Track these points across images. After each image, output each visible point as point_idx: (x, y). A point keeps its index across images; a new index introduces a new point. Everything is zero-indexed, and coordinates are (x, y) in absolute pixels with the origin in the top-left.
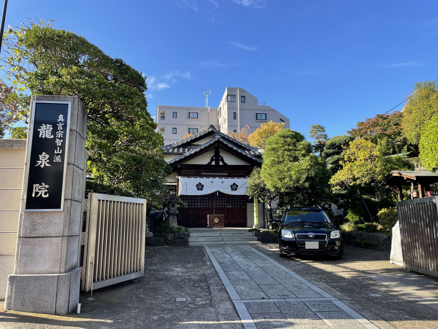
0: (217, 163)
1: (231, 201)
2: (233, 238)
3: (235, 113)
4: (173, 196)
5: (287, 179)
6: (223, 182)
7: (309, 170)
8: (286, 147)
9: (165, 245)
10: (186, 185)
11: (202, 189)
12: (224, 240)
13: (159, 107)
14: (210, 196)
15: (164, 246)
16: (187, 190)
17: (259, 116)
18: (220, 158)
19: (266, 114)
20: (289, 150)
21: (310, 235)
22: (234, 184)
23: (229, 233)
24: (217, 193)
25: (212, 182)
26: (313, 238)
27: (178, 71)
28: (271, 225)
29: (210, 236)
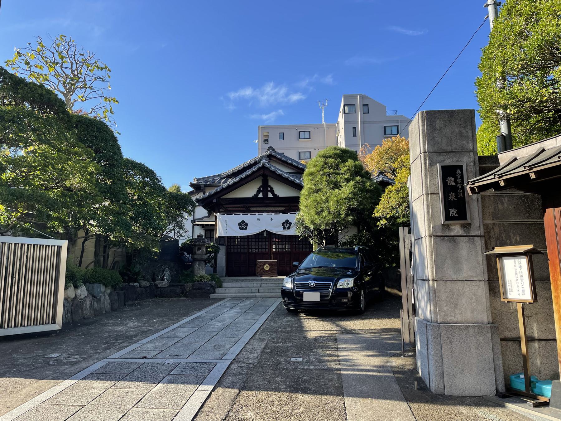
0: (265, 195)
2: (271, 289)
3: (355, 129)
4: (200, 238)
5: (325, 213)
6: (272, 219)
7: (350, 199)
8: (326, 170)
9: (182, 297)
10: (226, 224)
11: (245, 229)
12: (260, 292)
13: (261, 127)
14: (253, 237)
15: (181, 297)
16: (226, 229)
17: (388, 130)
18: (269, 189)
19: (398, 126)
20: (329, 175)
21: (310, 284)
22: (287, 221)
23: (272, 284)
24: (265, 233)
25: (258, 219)
26: (314, 287)
27: (316, 76)
29: (248, 286)
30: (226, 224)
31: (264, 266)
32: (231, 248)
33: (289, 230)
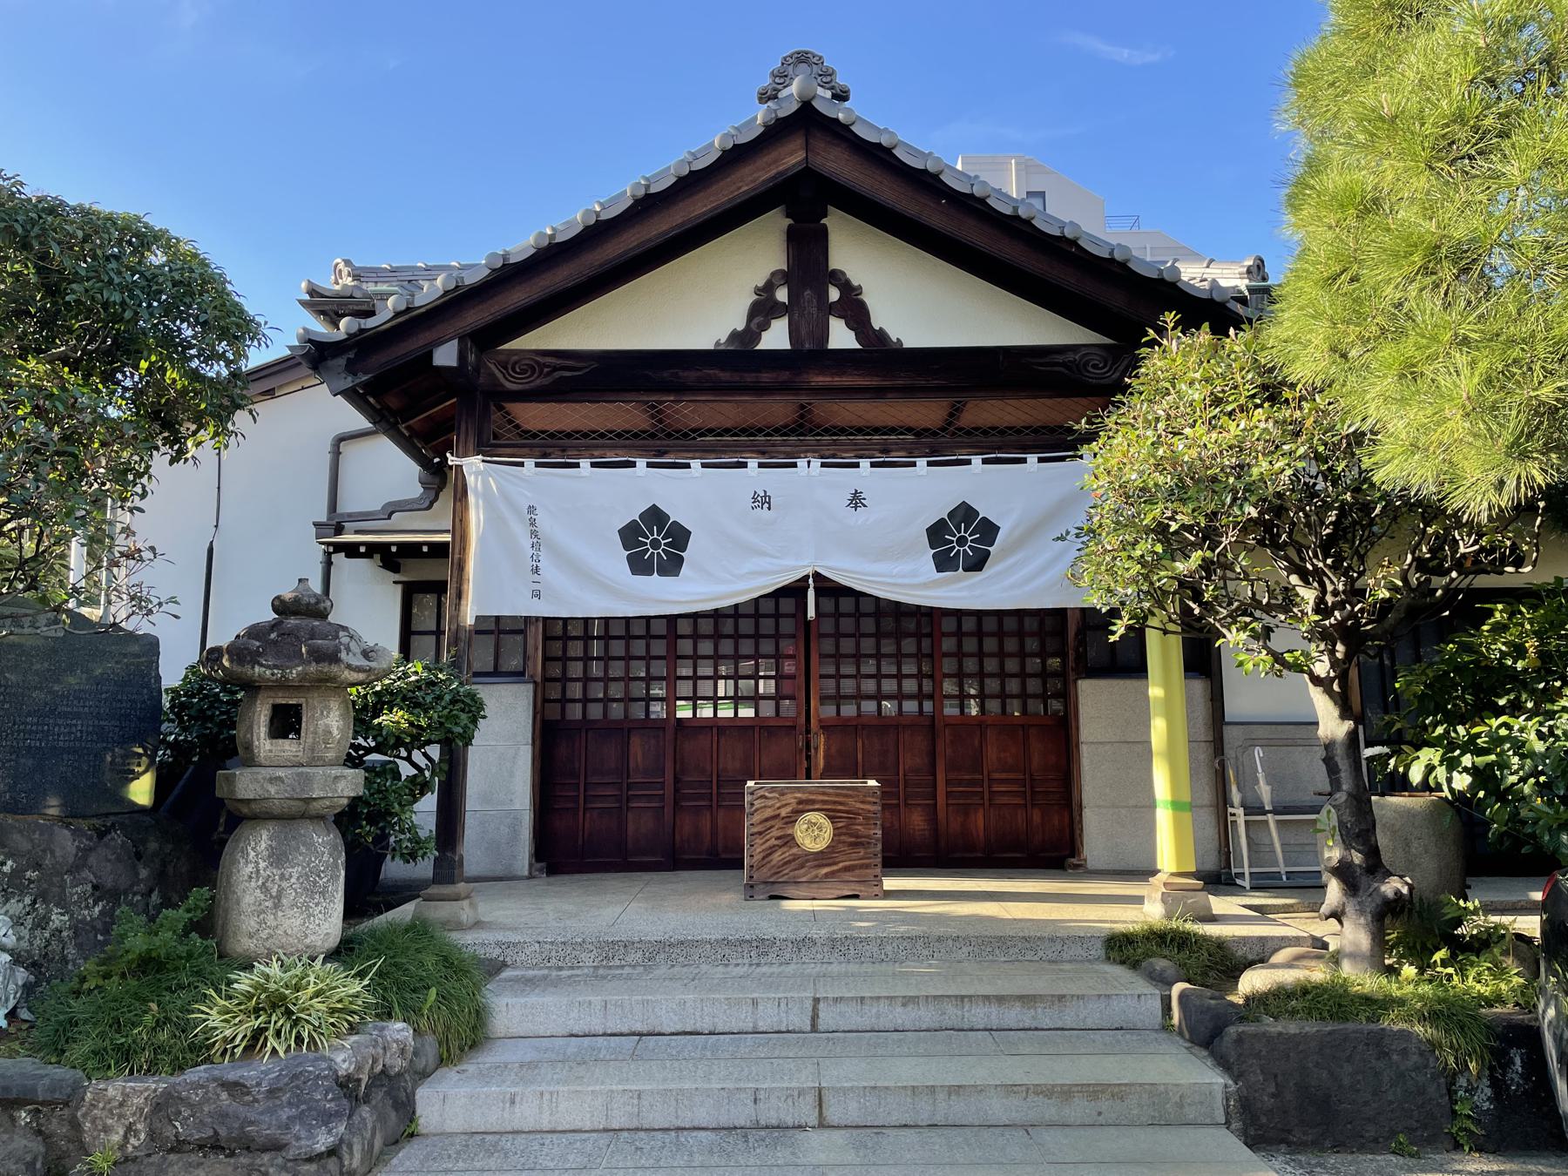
1: (948, 665)
4: (292, 621)
6: (856, 500)
10: (534, 534)
11: (672, 566)
12: (834, 1114)
16: (536, 570)
18: (834, 294)
22: (964, 513)
23: (908, 1001)
24: (811, 594)
25: (763, 501)
28: (1361, 912)
30: (534, 534)
31: (791, 820)
32: (564, 701)
33: (976, 577)
